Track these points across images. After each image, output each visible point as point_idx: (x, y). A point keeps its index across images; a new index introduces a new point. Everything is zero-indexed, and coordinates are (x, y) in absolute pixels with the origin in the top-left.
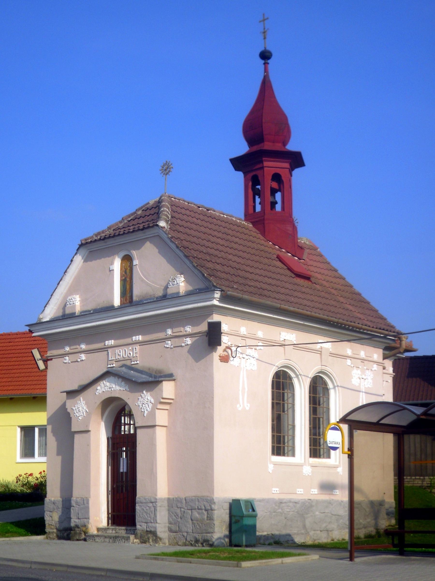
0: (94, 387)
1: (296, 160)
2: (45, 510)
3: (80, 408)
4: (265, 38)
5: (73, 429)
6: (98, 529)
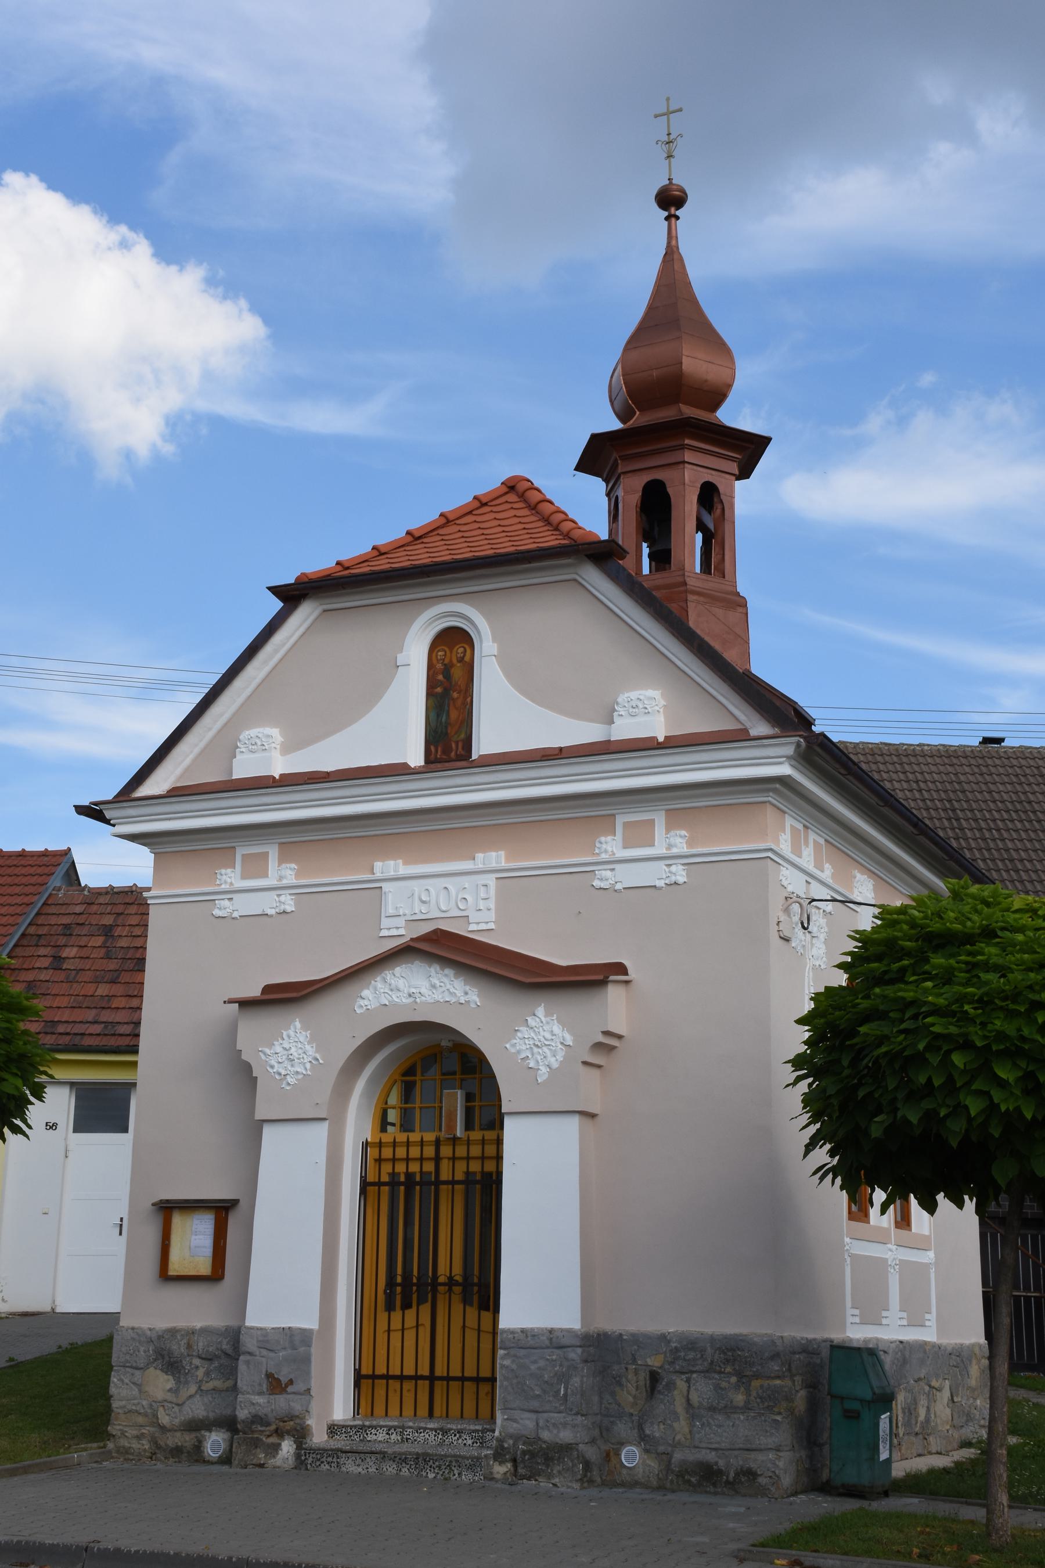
0: (347, 990)
1: (748, 449)
2: (114, 1360)
3: (291, 1052)
4: (670, 156)
5: (258, 1116)
6: (333, 1429)
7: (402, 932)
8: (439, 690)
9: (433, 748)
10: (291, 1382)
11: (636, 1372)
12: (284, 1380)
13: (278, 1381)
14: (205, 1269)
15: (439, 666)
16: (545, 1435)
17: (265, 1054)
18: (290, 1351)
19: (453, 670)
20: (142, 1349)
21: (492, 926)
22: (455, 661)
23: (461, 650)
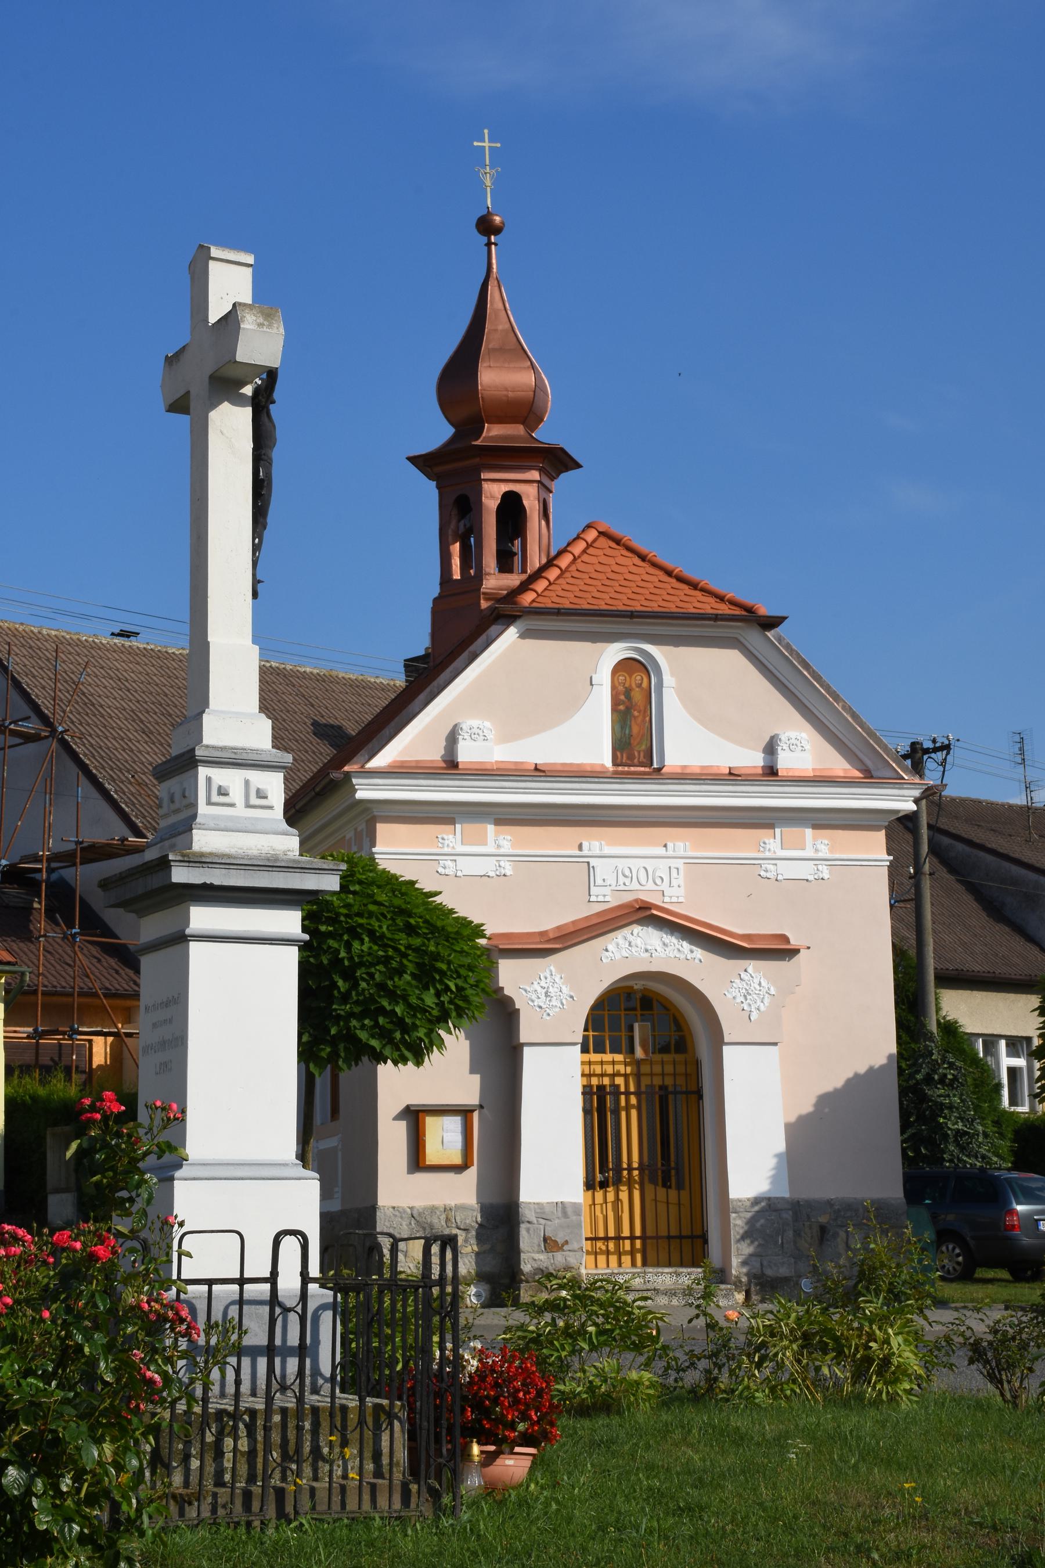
7: (607, 899)
8: (622, 707)
9: (619, 754)
10: (567, 1242)
11: (810, 1227)
12: (560, 1241)
13: (556, 1242)
14: (457, 1160)
15: (621, 688)
16: (769, 1272)
17: (526, 991)
18: (563, 1220)
19: (632, 694)
20: (404, 1223)
21: (681, 899)
22: (634, 686)
23: (639, 678)
